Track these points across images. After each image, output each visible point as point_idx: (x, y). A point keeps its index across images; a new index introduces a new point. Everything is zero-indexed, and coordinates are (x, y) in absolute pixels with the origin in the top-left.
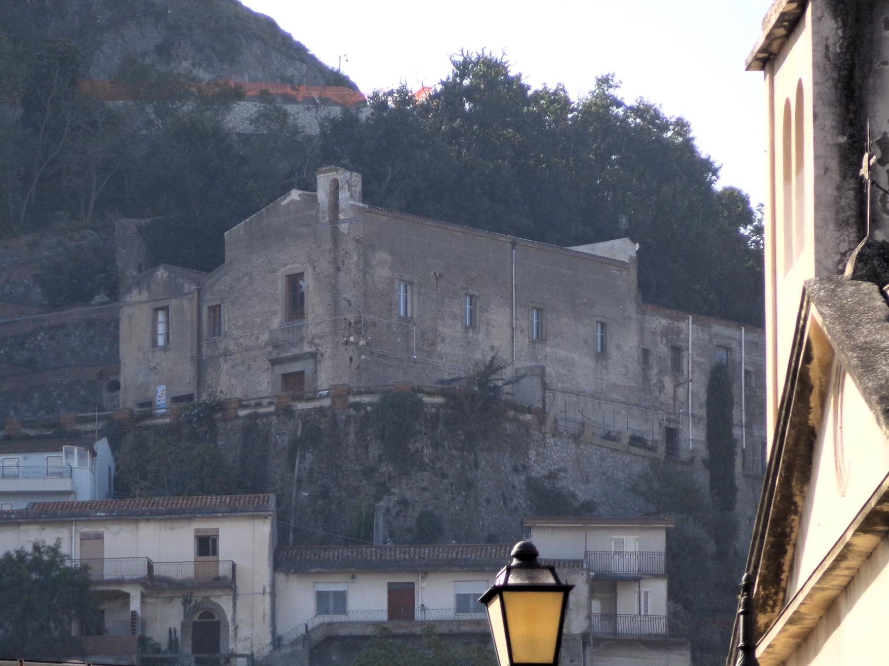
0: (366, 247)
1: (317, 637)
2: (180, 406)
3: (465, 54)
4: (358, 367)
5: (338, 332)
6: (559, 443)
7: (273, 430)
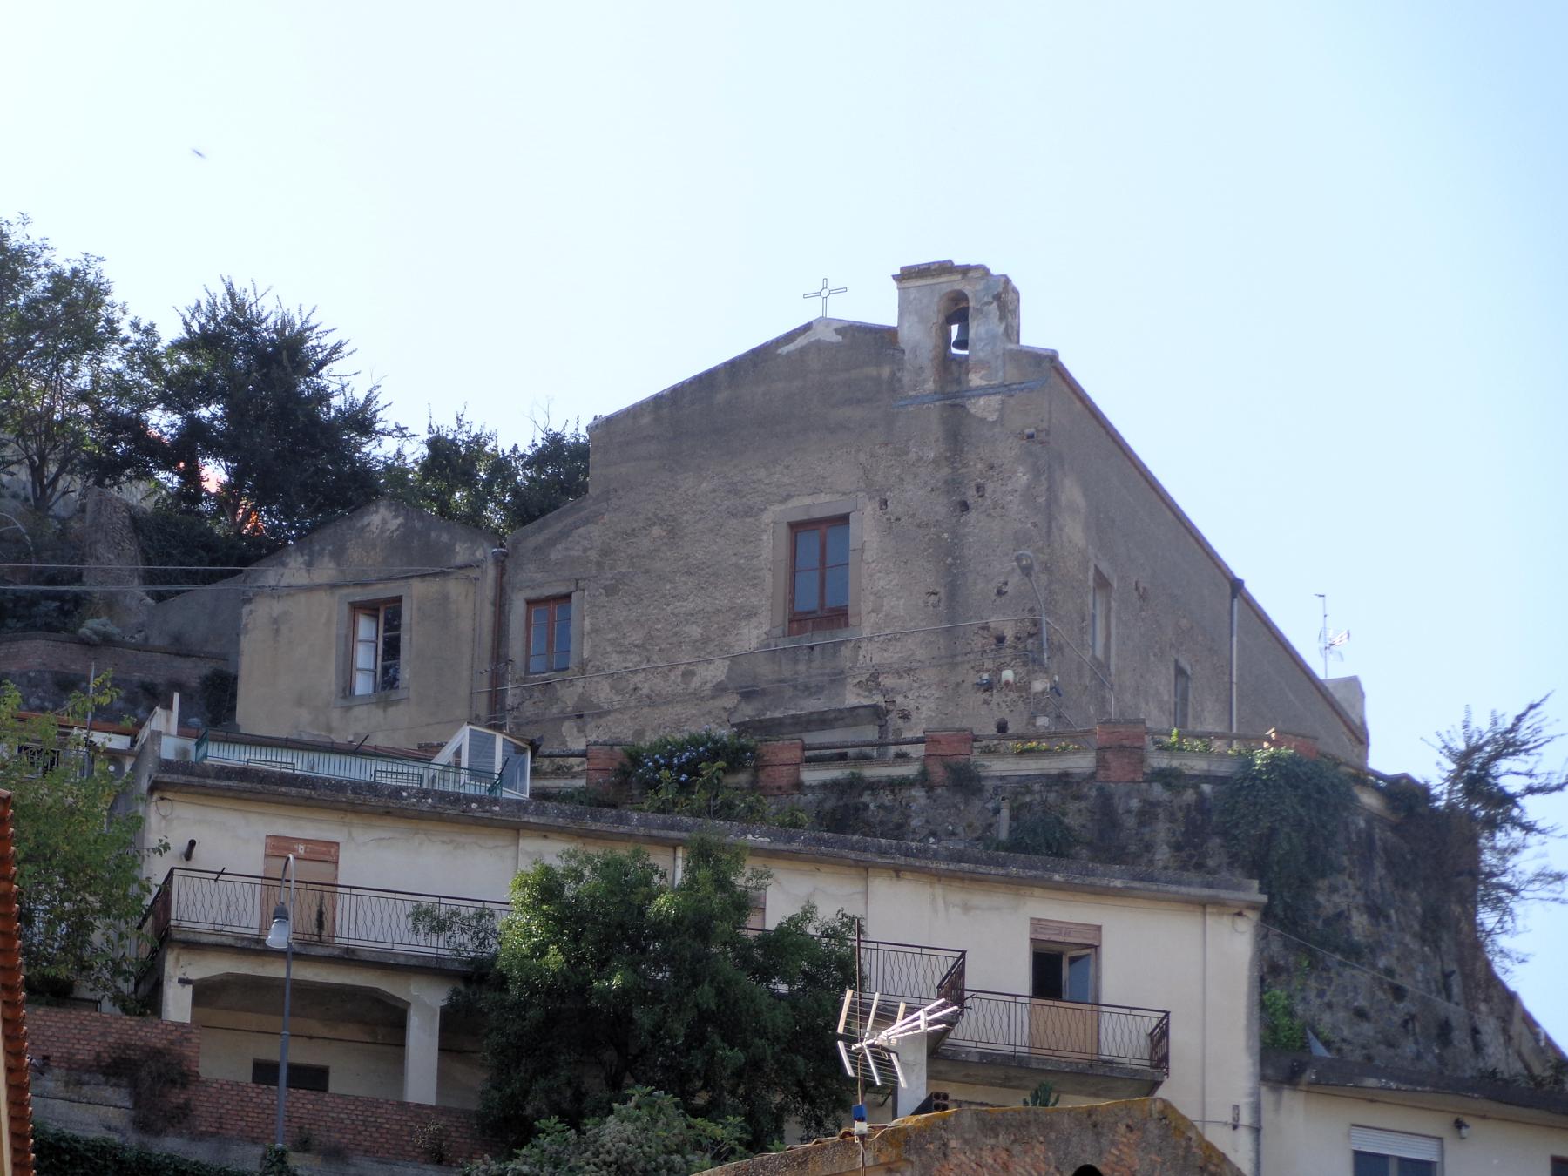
5: (959, 659)
7: (915, 822)
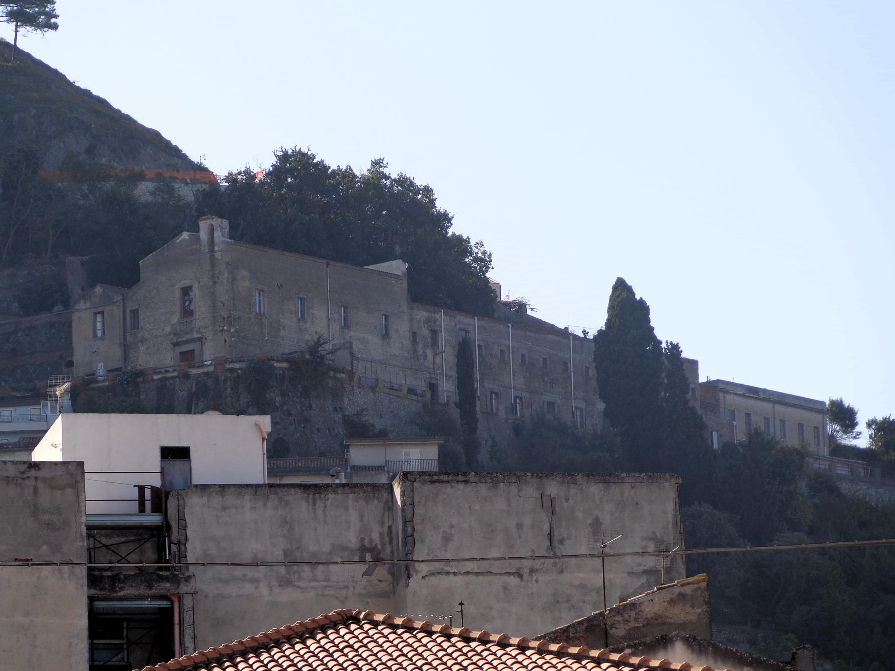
2: (115, 374)
3: (284, 150)
4: (230, 346)
6: (362, 392)
7: (177, 388)
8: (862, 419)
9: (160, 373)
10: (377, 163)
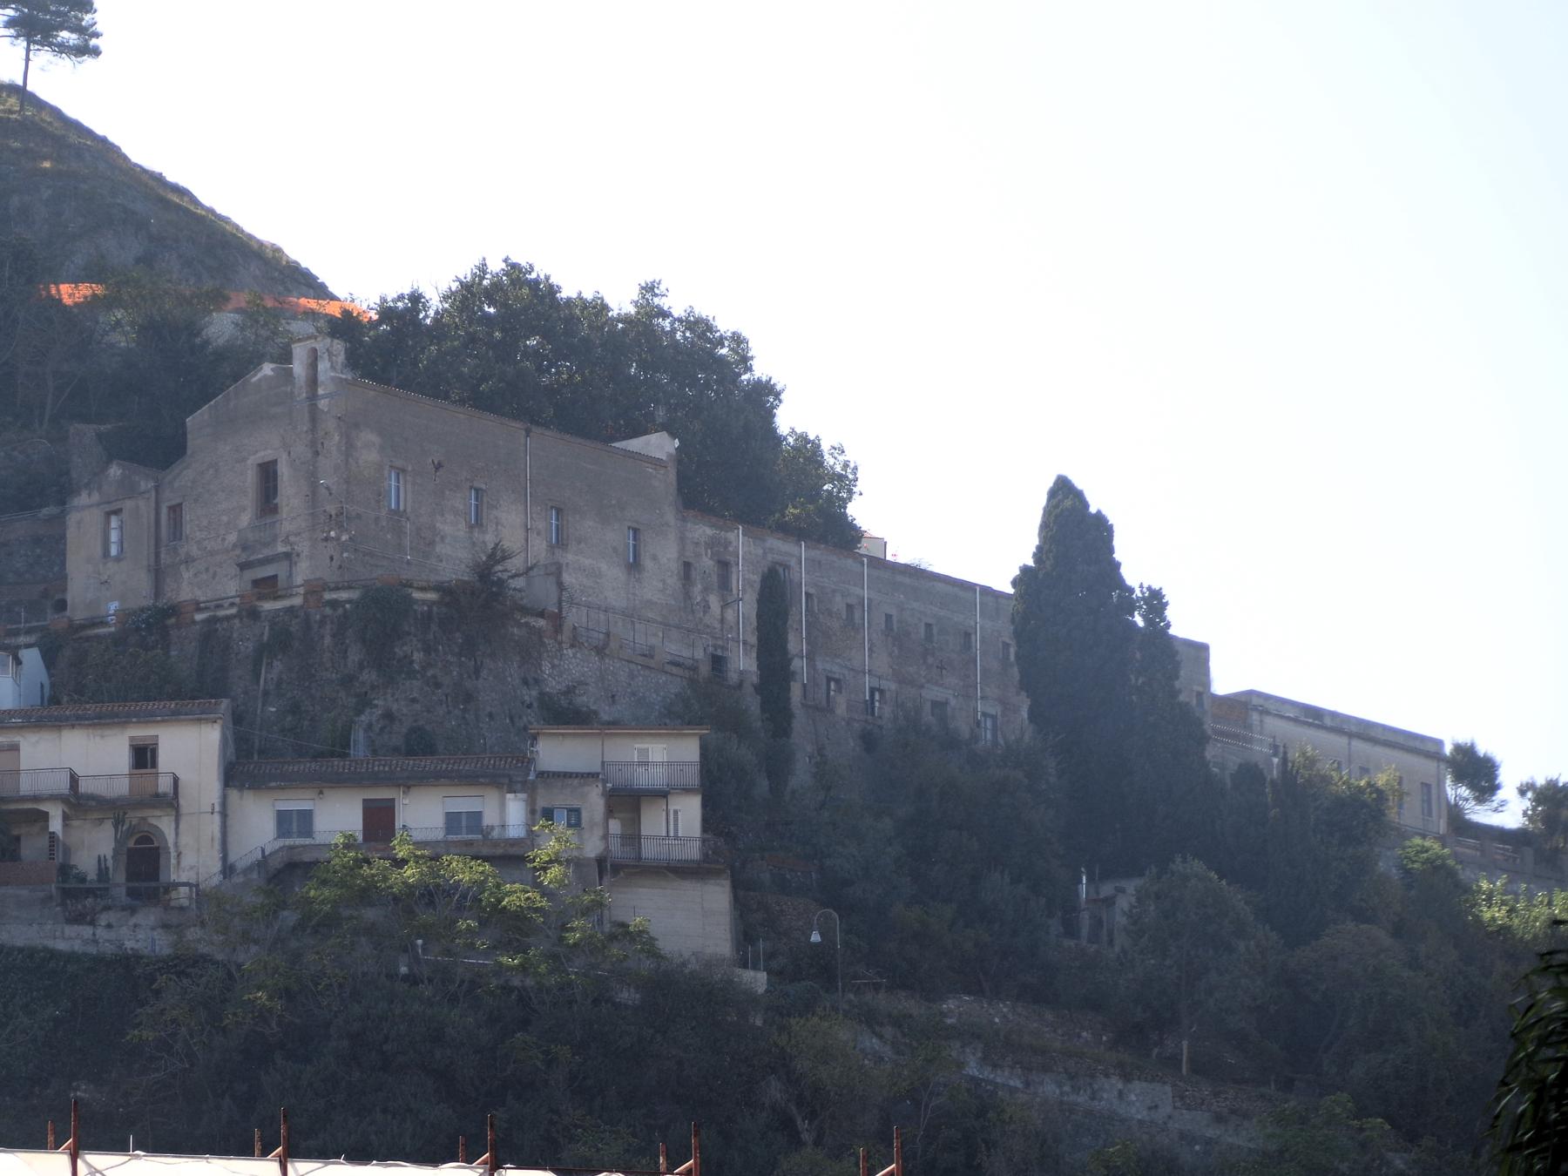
0: (350, 425)
1: (276, 863)
4: (340, 567)
7: (235, 635)
8: (1509, 779)
9: (206, 608)
10: (650, 289)
